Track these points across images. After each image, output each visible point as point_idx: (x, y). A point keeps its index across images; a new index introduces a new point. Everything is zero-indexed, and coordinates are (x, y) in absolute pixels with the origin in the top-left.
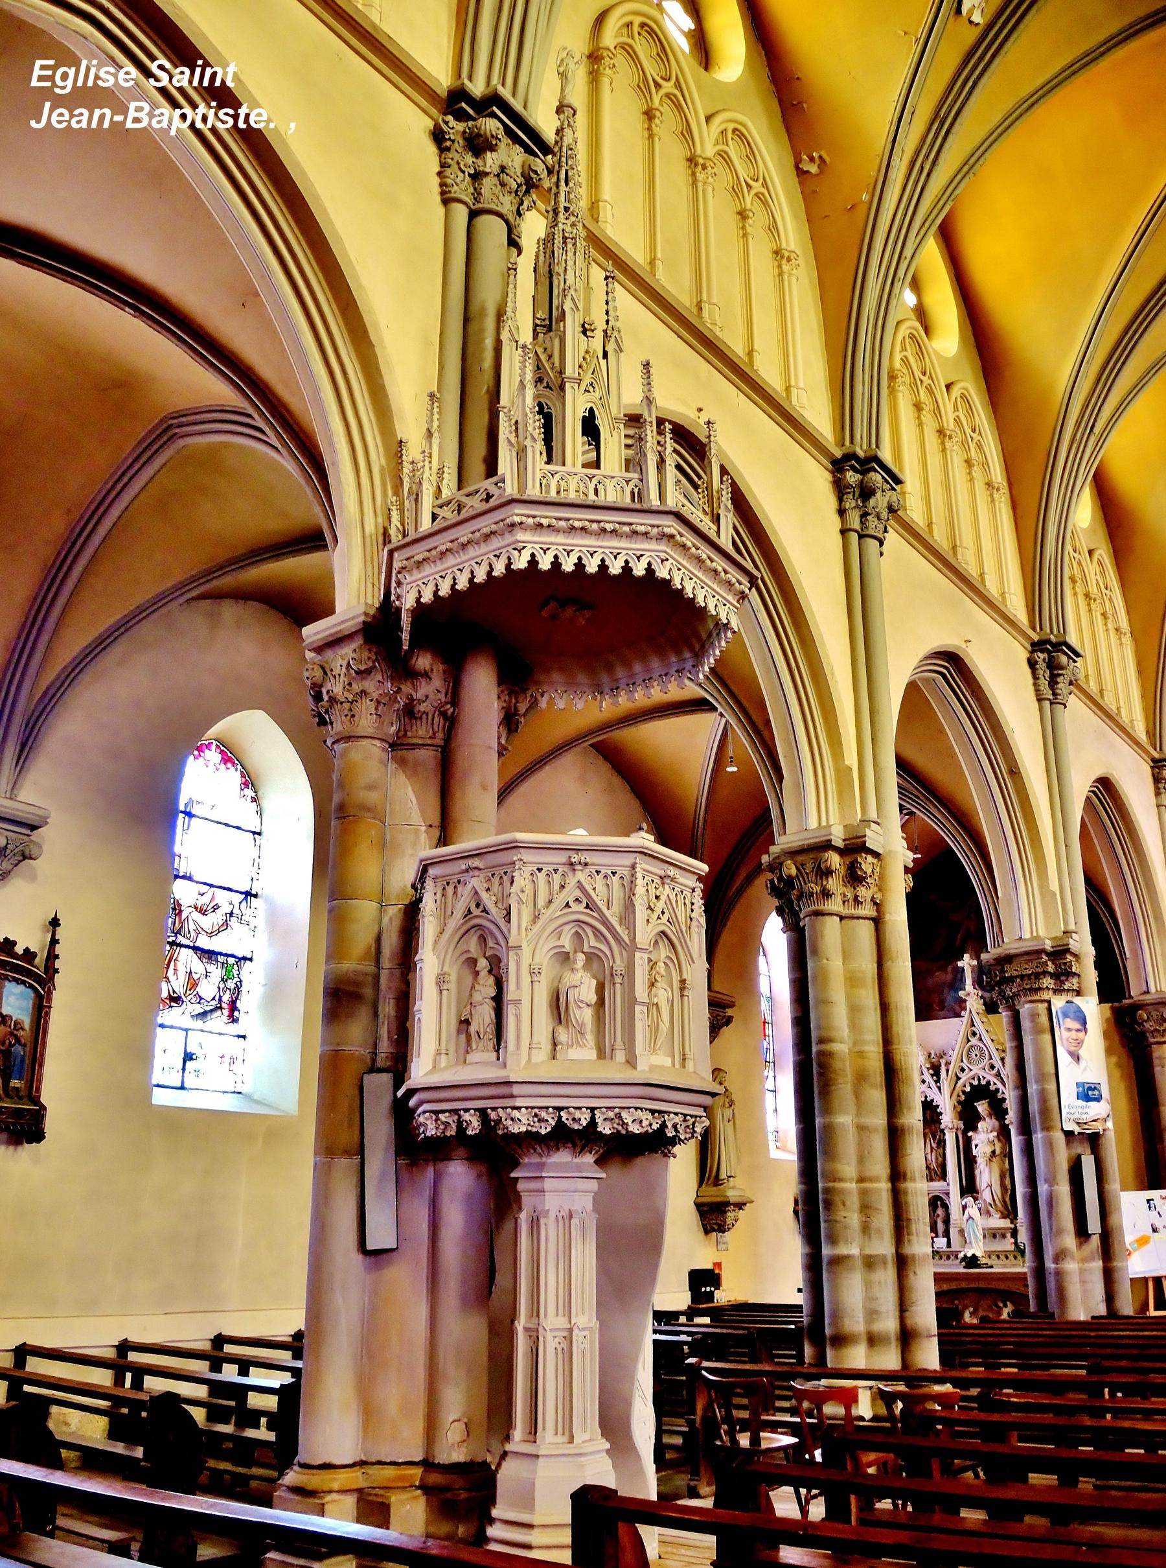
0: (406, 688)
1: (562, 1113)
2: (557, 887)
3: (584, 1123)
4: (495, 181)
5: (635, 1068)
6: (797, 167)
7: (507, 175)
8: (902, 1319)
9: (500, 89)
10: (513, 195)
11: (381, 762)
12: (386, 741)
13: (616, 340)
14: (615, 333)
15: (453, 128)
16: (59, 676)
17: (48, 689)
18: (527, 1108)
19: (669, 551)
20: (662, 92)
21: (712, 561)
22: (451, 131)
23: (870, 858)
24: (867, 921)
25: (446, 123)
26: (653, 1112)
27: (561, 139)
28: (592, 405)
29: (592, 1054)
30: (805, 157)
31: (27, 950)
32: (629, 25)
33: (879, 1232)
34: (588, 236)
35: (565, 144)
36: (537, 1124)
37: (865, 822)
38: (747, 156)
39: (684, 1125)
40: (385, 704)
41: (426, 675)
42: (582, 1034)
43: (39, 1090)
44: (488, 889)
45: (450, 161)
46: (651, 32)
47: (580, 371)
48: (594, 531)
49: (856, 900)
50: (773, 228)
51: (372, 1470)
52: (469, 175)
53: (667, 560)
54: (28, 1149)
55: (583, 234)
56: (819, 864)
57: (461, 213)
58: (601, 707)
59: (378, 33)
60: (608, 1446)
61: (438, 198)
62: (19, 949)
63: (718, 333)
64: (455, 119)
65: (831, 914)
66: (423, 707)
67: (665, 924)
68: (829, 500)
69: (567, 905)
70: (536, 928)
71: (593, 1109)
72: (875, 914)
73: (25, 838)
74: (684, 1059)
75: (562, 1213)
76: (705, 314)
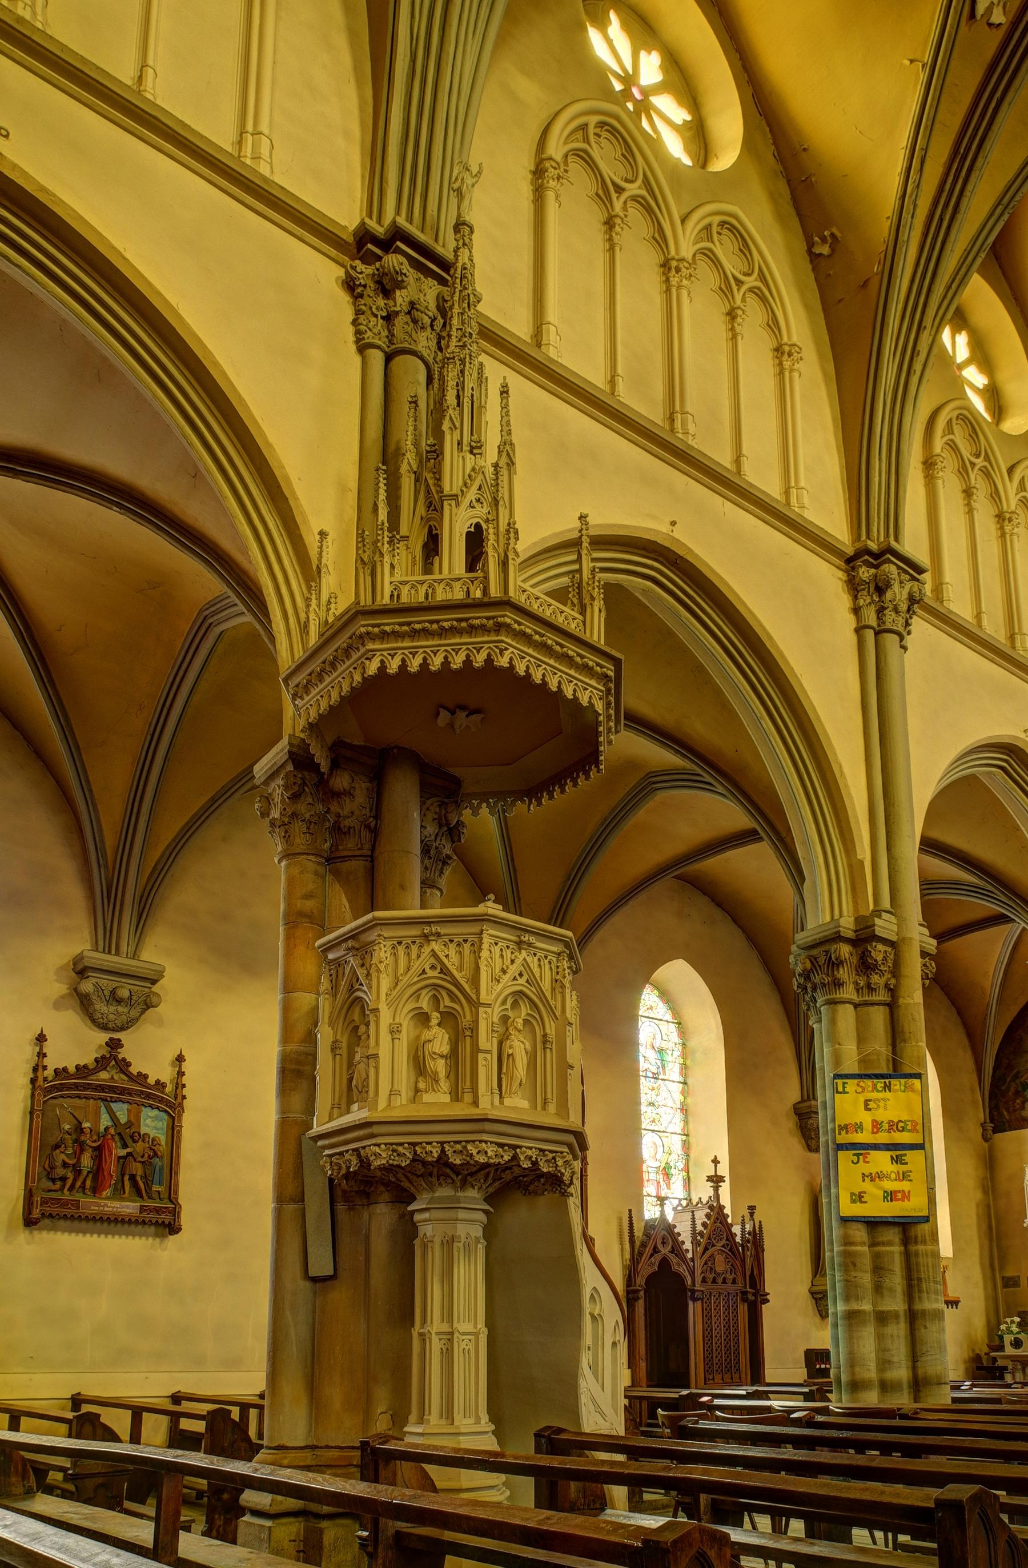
0: (334, 807)
1: (417, 1148)
2: (414, 956)
3: (436, 1155)
4: (407, 318)
5: (478, 1107)
6: (810, 252)
7: (417, 310)
8: (914, 1369)
10: (429, 329)
11: (316, 873)
13: (508, 454)
14: (508, 447)
15: (361, 273)
16: (164, 853)
17: (156, 865)
18: (386, 1144)
19: (509, 641)
20: (625, 196)
22: (360, 276)
23: (880, 947)
24: (881, 1007)
25: (354, 268)
26: (501, 1145)
28: (475, 521)
29: (446, 1099)
30: (816, 239)
31: (158, 1082)
33: (891, 1290)
36: (397, 1158)
37: (877, 913)
39: (544, 1159)
41: (349, 793)
42: (437, 1082)
43: (176, 1192)
44: (363, 965)
46: (613, 131)
48: (434, 631)
49: (870, 988)
50: (773, 325)
51: (318, 1452)
52: (382, 317)
53: (507, 649)
54: (172, 1238)
56: (830, 957)
57: (377, 358)
58: (529, 809)
60: (493, 1427)
61: (353, 348)
62: (151, 1081)
63: (690, 442)
64: (363, 263)
65: (844, 1002)
66: (347, 823)
67: (523, 985)
68: (845, 601)
69: (424, 972)
70: (394, 993)
71: (442, 1143)
72: (888, 999)
73: (147, 990)
74: (545, 1103)
75: (447, 1238)
76: (678, 424)
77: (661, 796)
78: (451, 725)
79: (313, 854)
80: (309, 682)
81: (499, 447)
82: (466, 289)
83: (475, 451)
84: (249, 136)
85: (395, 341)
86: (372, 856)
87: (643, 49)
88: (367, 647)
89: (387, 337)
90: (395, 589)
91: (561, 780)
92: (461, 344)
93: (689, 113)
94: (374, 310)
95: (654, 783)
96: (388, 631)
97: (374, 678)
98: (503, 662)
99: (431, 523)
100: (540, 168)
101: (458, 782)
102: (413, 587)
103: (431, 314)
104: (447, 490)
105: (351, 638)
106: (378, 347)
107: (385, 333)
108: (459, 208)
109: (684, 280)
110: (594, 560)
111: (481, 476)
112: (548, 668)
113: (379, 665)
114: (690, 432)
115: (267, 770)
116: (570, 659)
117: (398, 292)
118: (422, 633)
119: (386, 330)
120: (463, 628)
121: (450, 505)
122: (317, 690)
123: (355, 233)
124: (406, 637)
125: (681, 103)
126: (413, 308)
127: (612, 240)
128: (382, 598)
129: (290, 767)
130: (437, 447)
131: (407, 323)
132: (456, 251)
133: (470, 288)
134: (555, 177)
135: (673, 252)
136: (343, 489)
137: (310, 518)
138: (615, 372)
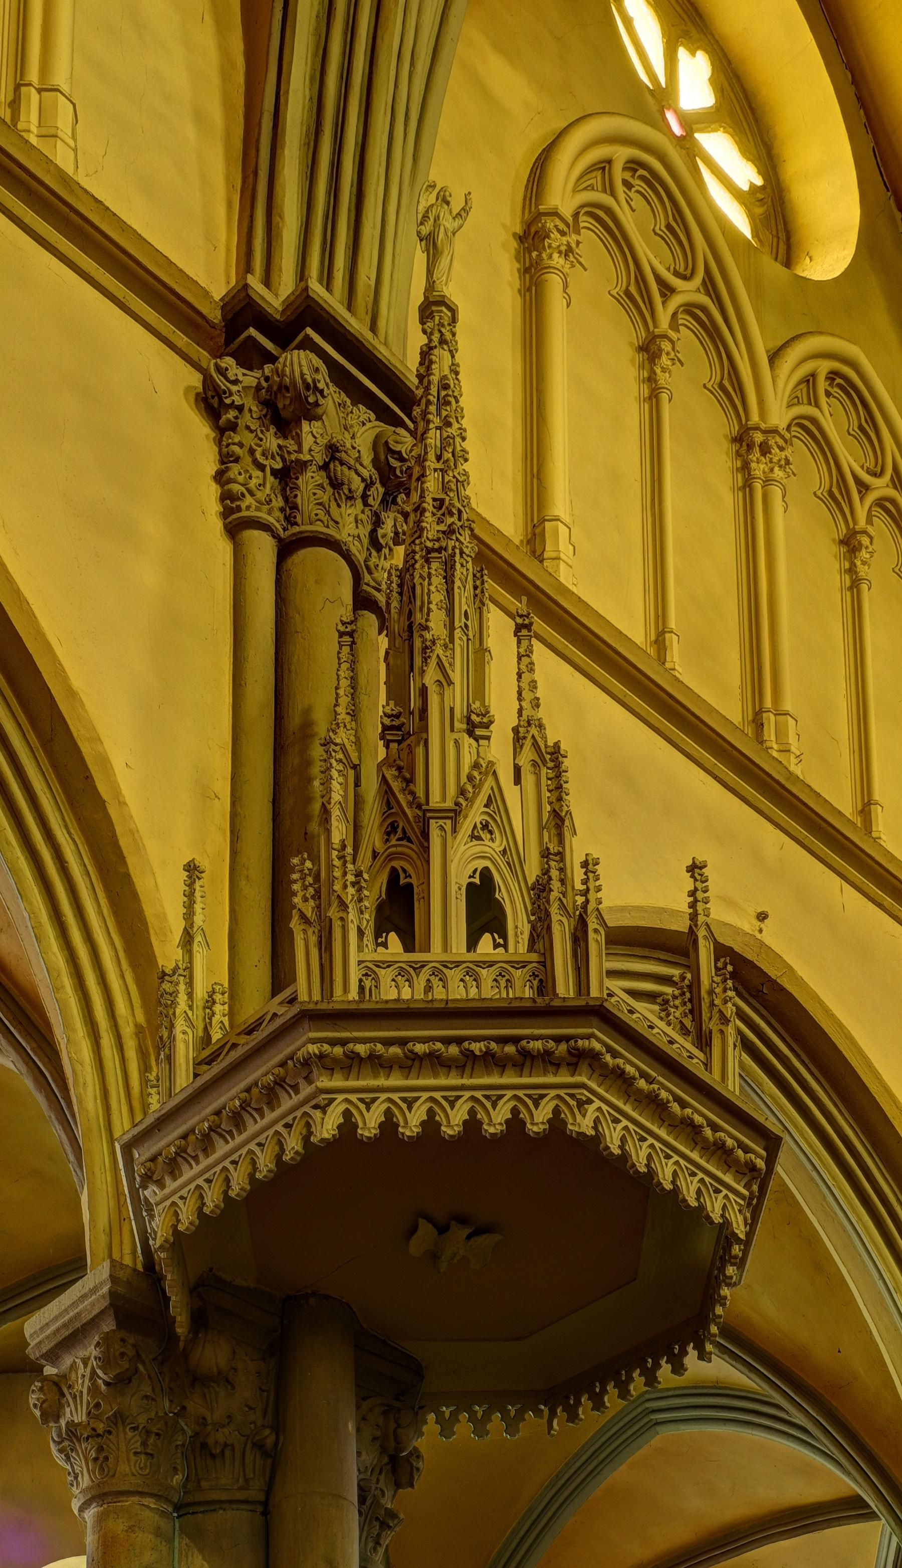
0: (196, 1406)
4: (320, 478)
7: (342, 463)
9: (317, 288)
11: (158, 1532)
12: (168, 1500)
14: (534, 731)
15: (236, 382)
19: (593, 1085)
20: (676, 301)
21: (683, 1105)
22: (234, 388)
25: (222, 372)
27: (429, 368)
28: (481, 864)
32: (604, 166)
34: (479, 554)
35: (435, 379)
38: (861, 427)
40: (157, 1434)
41: (226, 1380)
45: (236, 449)
46: (653, 180)
47: (461, 800)
48: (452, 1059)
55: (470, 547)
59: (72, 192)
61: (217, 525)
63: (792, 768)
64: (241, 364)
76: (770, 734)
77: (667, 1433)
78: (434, 1256)
79: (153, 1495)
80: (181, 1152)
81: (516, 730)
82: (449, 424)
83: (479, 732)
84: (33, 92)
85: (299, 520)
86: (265, 1504)
87: (682, 44)
88: (320, 1084)
89: (282, 510)
90: (366, 975)
91: (618, 1373)
92: (442, 527)
93: (759, 173)
94: (258, 455)
95: (654, 1411)
96: (363, 1054)
97: (329, 1144)
98: (584, 1124)
99: (396, 864)
100: (533, 230)
101: (417, 1370)
102: (401, 972)
103: (366, 473)
104: (435, 800)
105: (283, 1064)
106: (266, 527)
107: (278, 502)
108: (430, 272)
109: (776, 469)
110: (612, 974)
111: (490, 781)
112: (657, 1145)
113: (341, 1120)
114: (793, 749)
115: (58, 1330)
116: (696, 1129)
117: (305, 426)
118: (426, 1063)
119: (280, 498)
120: (508, 1057)
121: (442, 828)
122: (197, 1169)
123: (226, 305)
124: (396, 1067)
125: (745, 152)
126: (333, 458)
127: (656, 381)
128: (346, 990)
129: (109, 1325)
130: (402, 719)
131: (321, 486)
132: (426, 354)
133: (456, 426)
134: (563, 248)
135: (755, 418)
136: (205, 795)
137: (147, 842)
138: (664, 626)
